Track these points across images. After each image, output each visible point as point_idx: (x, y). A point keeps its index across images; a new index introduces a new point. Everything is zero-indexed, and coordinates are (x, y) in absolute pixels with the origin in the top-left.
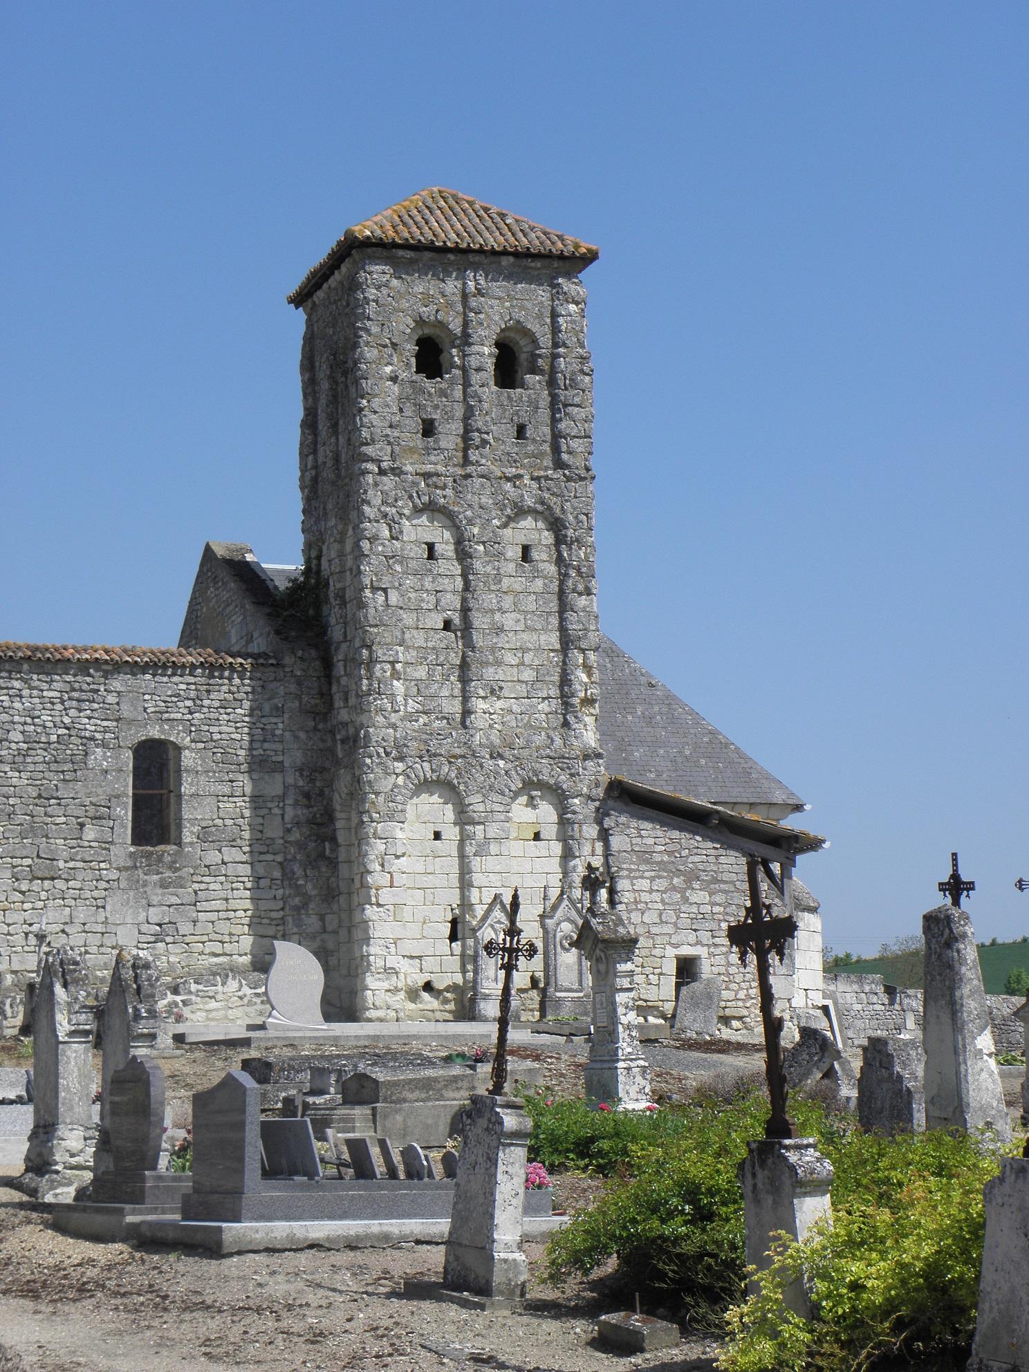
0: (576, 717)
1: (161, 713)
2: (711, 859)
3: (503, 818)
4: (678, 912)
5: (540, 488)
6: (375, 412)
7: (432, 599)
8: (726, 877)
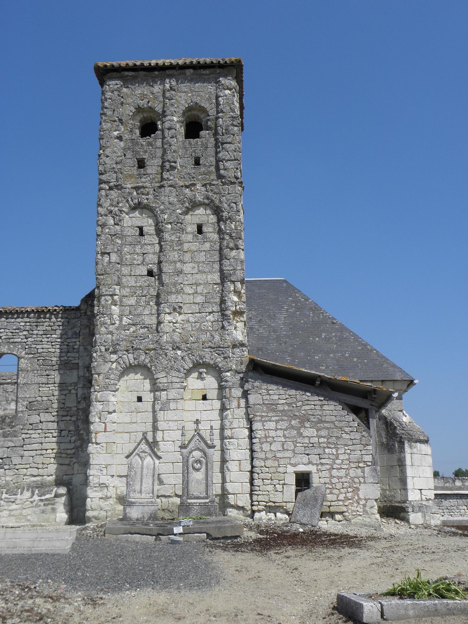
0: (228, 322)
1: (9, 339)
2: (317, 407)
3: (179, 386)
4: (295, 443)
5: (207, 191)
6: (107, 156)
7: (141, 258)
8: (328, 419)
